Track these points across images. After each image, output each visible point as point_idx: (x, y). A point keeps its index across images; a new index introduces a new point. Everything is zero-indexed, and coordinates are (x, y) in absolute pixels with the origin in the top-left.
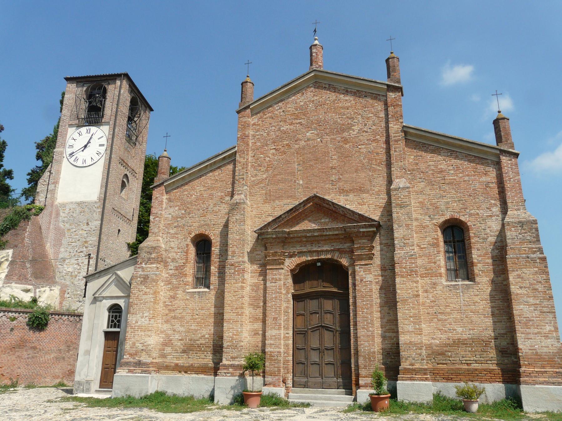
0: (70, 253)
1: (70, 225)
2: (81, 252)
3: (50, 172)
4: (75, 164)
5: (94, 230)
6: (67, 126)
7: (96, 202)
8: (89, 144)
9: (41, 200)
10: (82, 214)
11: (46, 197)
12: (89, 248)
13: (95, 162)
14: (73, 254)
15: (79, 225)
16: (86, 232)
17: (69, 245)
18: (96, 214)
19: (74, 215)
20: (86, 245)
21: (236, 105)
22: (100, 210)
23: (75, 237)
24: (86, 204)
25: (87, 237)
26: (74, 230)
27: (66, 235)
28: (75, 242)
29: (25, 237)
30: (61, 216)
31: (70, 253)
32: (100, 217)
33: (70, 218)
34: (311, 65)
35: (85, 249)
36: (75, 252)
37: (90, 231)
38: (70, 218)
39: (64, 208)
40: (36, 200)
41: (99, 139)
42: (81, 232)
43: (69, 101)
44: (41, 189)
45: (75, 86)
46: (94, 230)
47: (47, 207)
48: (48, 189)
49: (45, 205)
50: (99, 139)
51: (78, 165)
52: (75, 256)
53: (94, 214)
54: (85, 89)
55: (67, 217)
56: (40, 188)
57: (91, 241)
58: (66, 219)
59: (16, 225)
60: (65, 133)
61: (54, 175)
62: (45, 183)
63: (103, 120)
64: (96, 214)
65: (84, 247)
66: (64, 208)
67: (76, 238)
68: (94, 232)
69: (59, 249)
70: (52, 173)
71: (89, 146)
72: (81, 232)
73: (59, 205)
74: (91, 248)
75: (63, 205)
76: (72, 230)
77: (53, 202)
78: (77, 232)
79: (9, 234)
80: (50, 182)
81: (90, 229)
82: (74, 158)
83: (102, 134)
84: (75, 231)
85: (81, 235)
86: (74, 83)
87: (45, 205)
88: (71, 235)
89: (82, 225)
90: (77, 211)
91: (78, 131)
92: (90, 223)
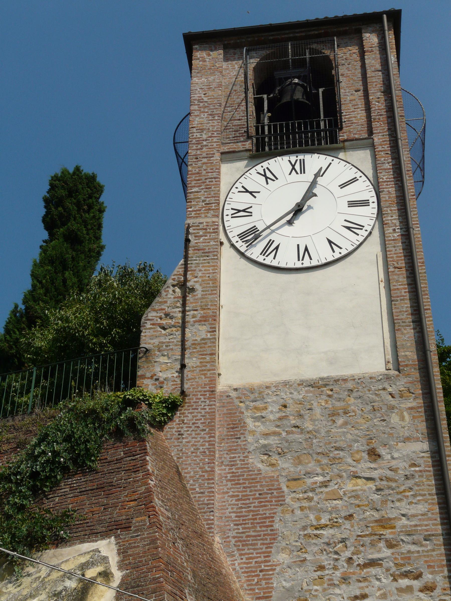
0: (322, 568)
1: (298, 461)
2: (373, 563)
3: (183, 285)
4: (269, 261)
5: (407, 477)
6: (217, 156)
7: (388, 378)
8: (308, 203)
9: (162, 376)
10: (340, 421)
11: (183, 366)
12: (405, 548)
13: (344, 252)
14: (338, 574)
15: (335, 461)
16: (371, 485)
17: (308, 536)
18: (402, 418)
19: (308, 426)
20: (388, 534)
21: (311, 210)
22: (414, 404)
23: (329, 505)
24: (350, 385)
25: (384, 502)
26: (320, 479)
27: (288, 500)
28: (334, 524)
29: (149, 491)
30: (253, 432)
31: (322, 568)
32: (422, 426)
33: (291, 437)
34: (390, 369)
35: (387, 552)
36: (342, 563)
37: (388, 479)
38: (291, 437)
39: (258, 404)
40: (143, 377)
41: (342, 186)
42: (349, 486)
43: (210, 93)
44: (156, 341)
45: (222, 56)
46: (407, 477)
47: (191, 399)
48: (183, 341)
49: (183, 393)
50: (342, 186)
51: (283, 265)
52: (345, 579)
53: (395, 419)
54: (253, 62)
55: (279, 434)
56: (152, 337)
57: (404, 521)
58: (273, 441)
59: (88, 454)
60: (215, 175)
61: (199, 293)
62: (172, 322)
63: (343, 136)
64: (402, 418)
65: (382, 544)
66: (258, 404)
67: (335, 509)
68: (410, 483)
69: (268, 555)
70: (193, 290)
71: (310, 207)
72: (349, 486)
73: (233, 394)
74: (413, 548)
75: (252, 390)
76: (309, 481)
77: (213, 382)
78: (332, 487)
79: (64, 488)
80: (188, 319)
81: (389, 474)
82: (261, 245)
83: (352, 173)
84: (325, 484)
85: (357, 497)
86: (216, 49)
87: (183, 393)
88: (310, 499)
89: (349, 460)
90: (318, 411)
91: (259, 168)
92: (382, 451)
